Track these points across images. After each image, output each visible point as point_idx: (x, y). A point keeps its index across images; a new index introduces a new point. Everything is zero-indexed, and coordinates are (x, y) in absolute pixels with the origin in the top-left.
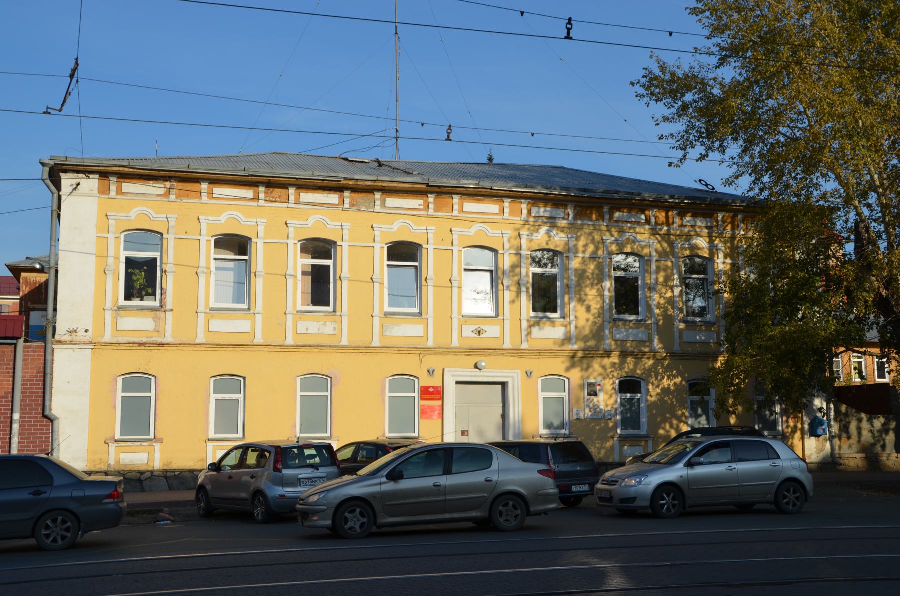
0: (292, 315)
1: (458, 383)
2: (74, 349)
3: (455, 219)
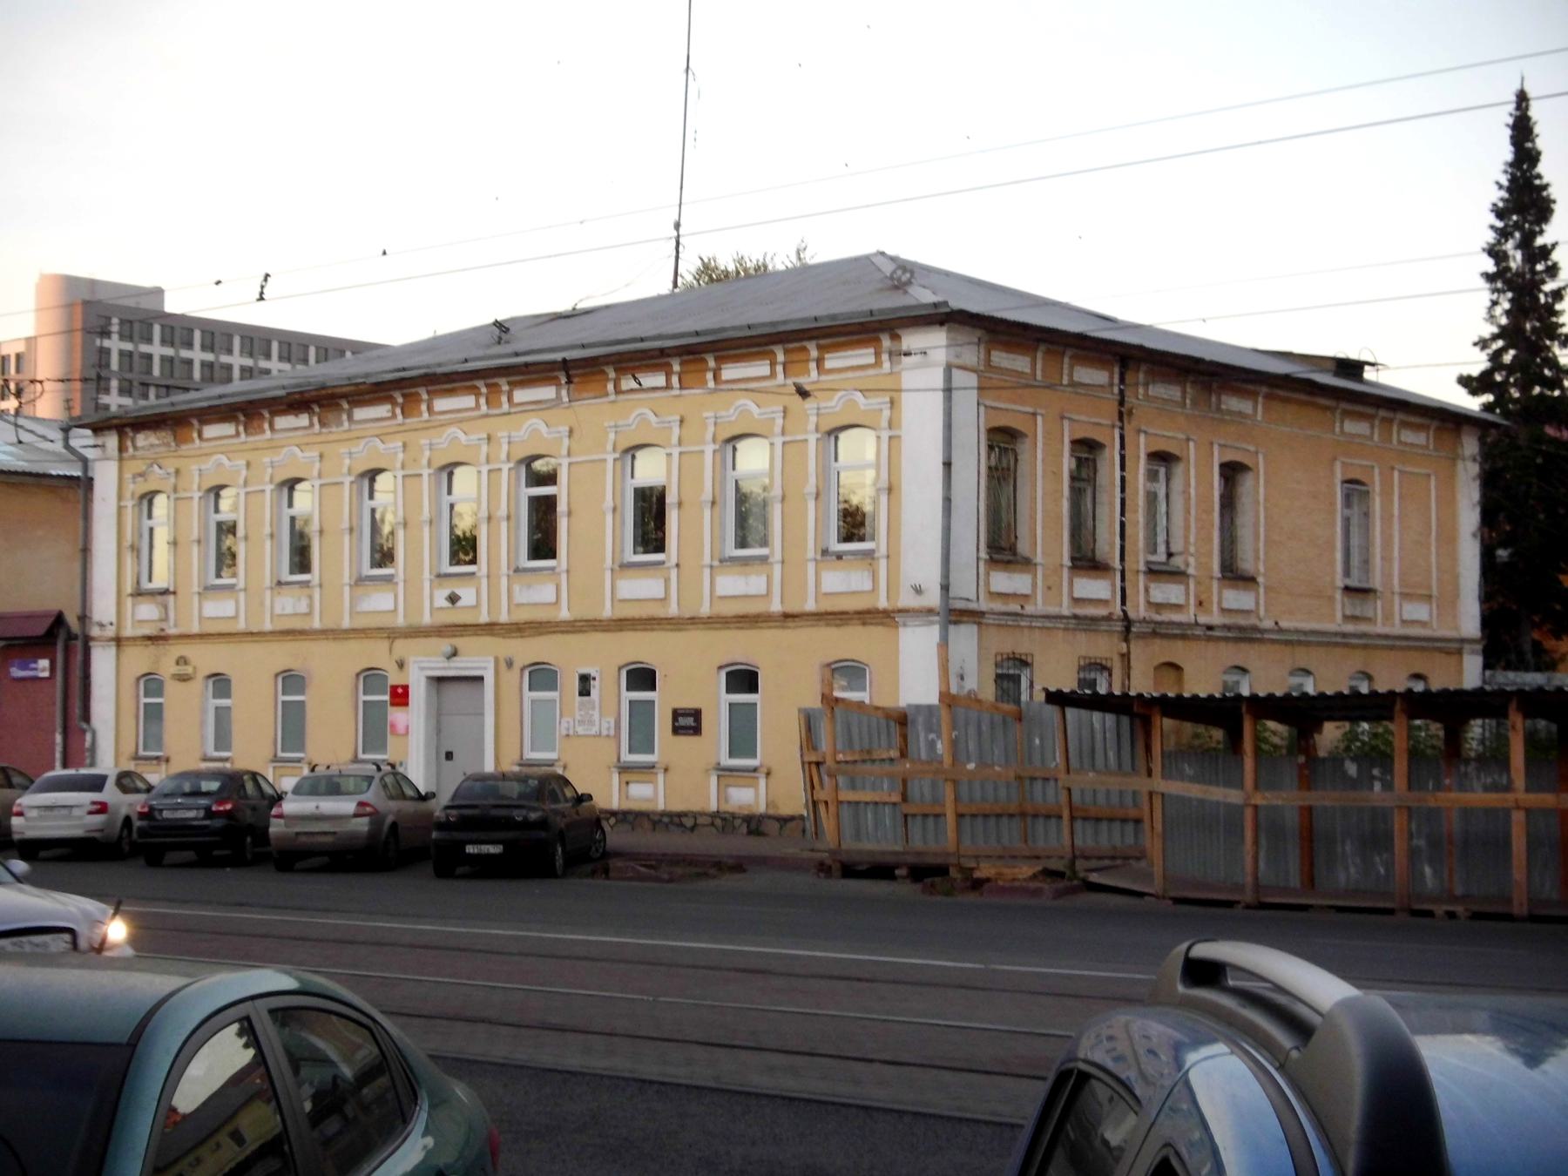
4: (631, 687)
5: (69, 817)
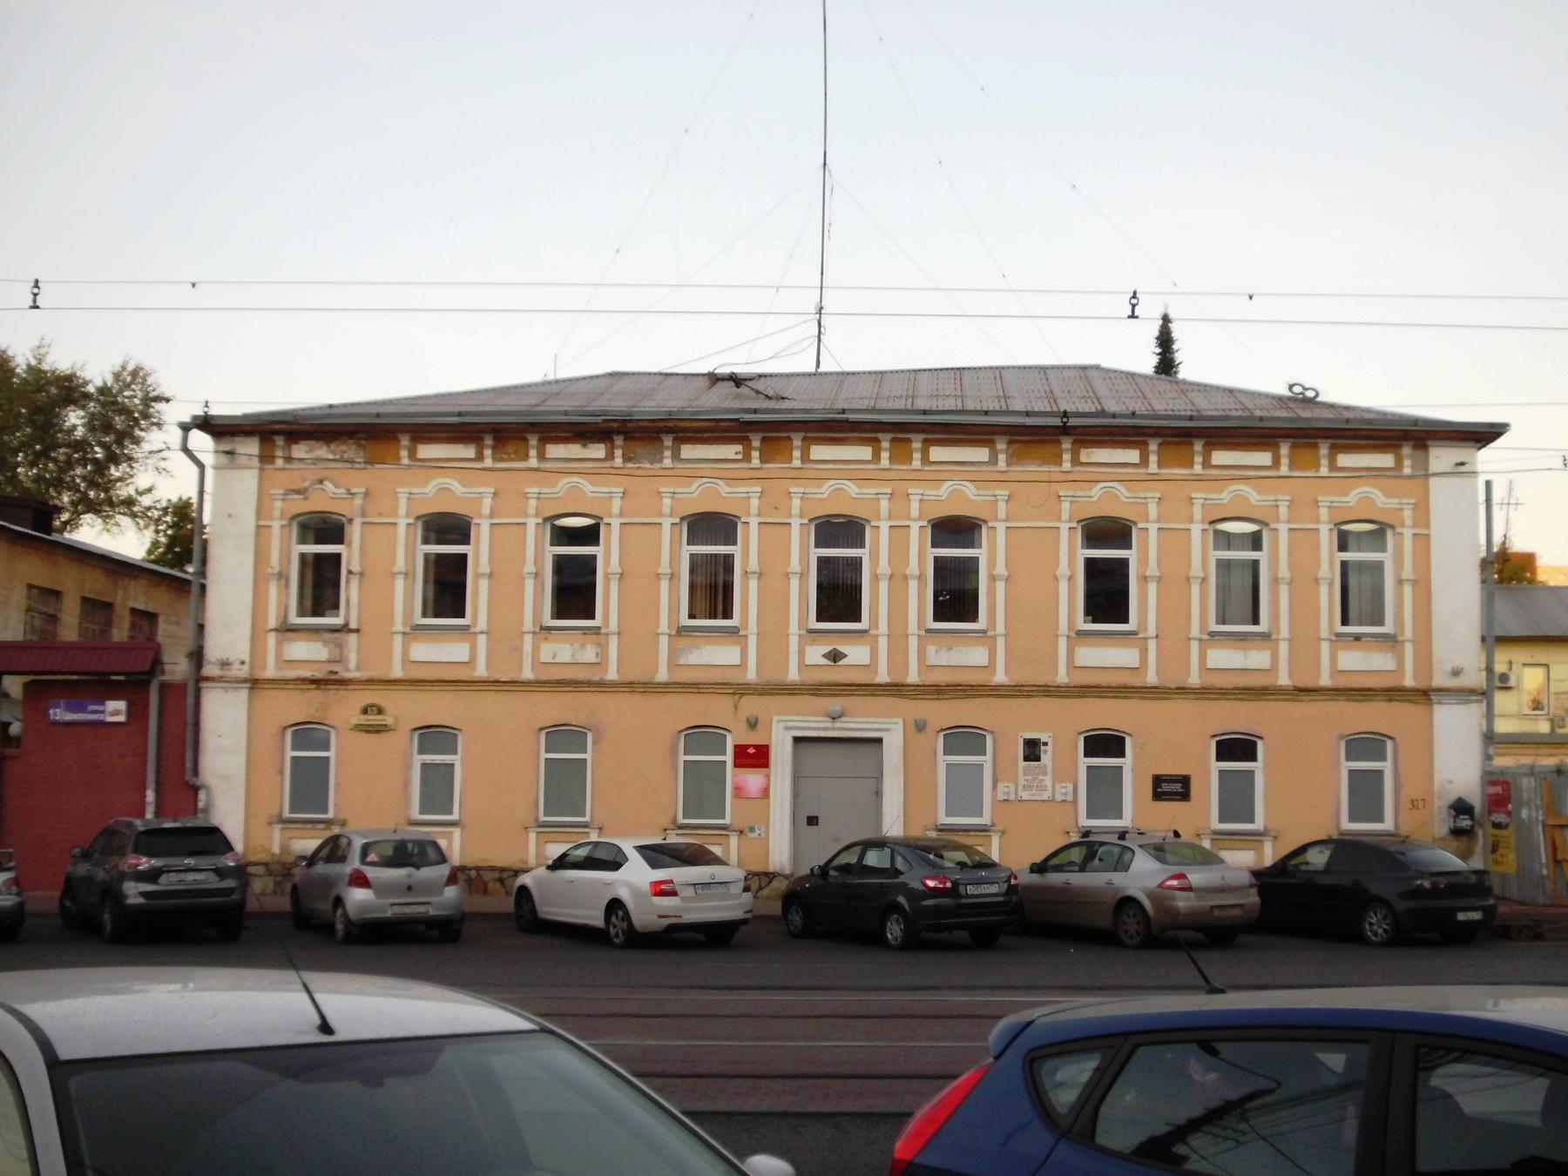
0: (531, 635)
1: (797, 740)
2: (225, 689)
3: (1200, 479)
4: (1221, 757)
5: (726, 896)
